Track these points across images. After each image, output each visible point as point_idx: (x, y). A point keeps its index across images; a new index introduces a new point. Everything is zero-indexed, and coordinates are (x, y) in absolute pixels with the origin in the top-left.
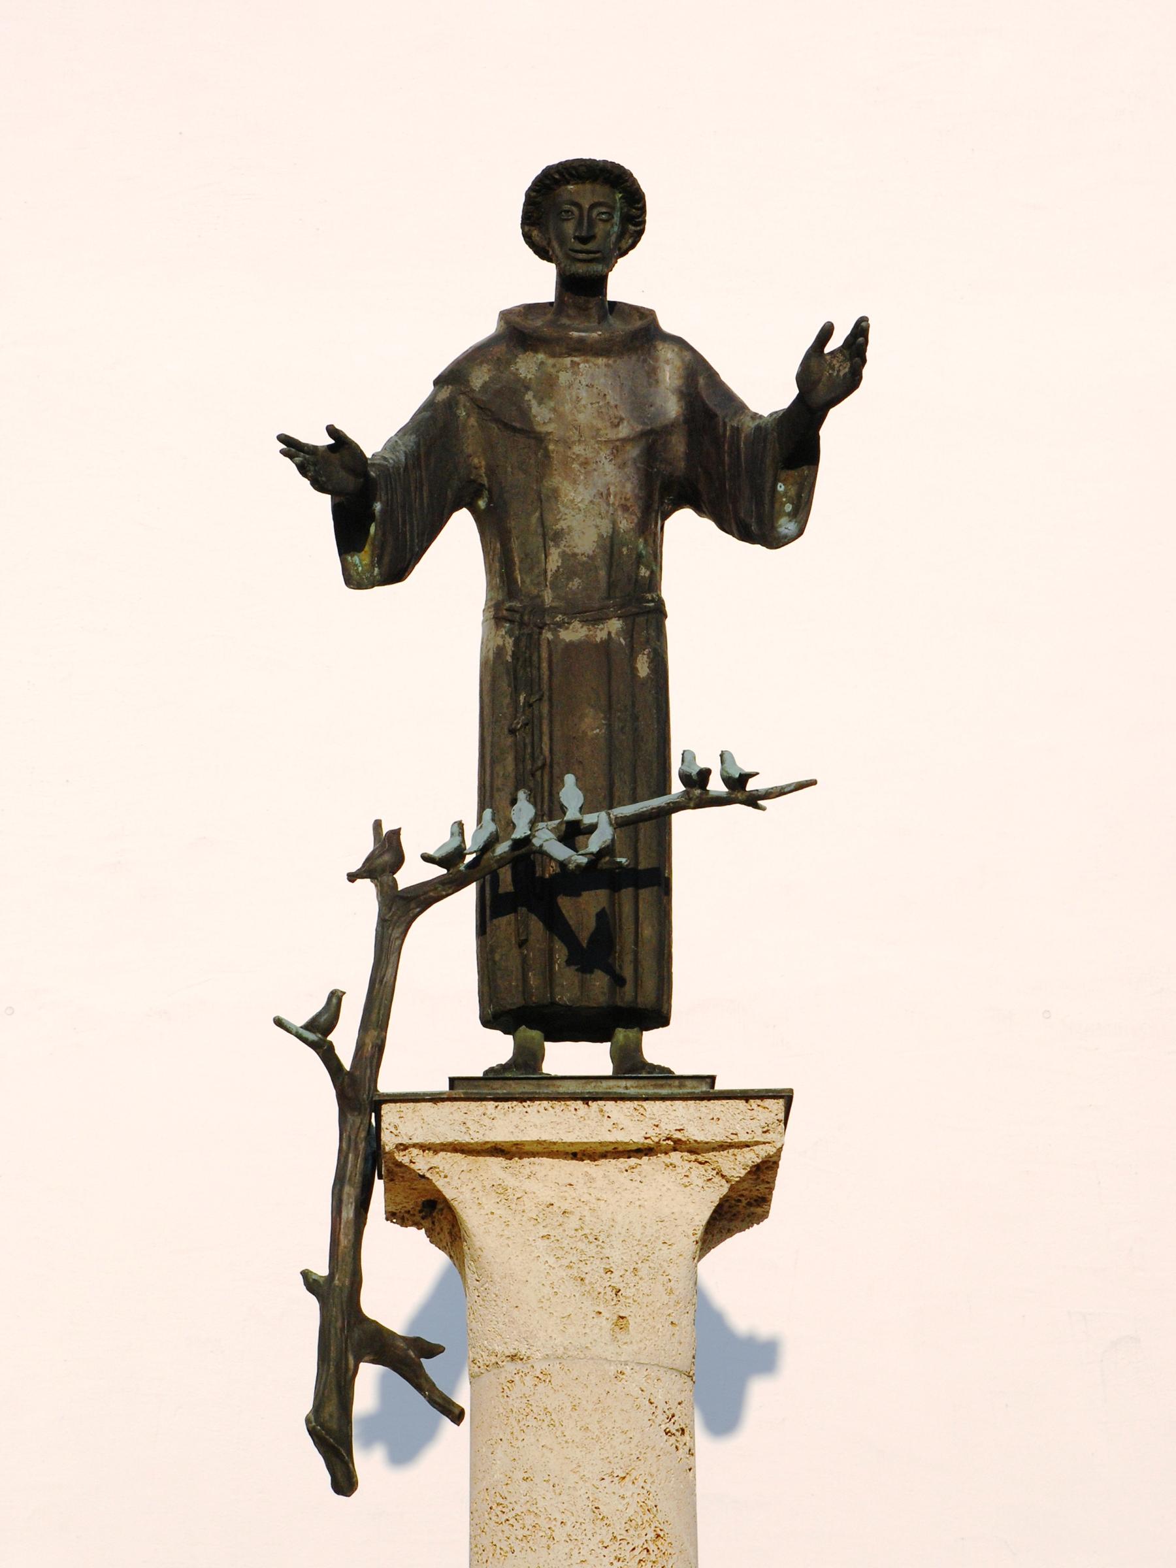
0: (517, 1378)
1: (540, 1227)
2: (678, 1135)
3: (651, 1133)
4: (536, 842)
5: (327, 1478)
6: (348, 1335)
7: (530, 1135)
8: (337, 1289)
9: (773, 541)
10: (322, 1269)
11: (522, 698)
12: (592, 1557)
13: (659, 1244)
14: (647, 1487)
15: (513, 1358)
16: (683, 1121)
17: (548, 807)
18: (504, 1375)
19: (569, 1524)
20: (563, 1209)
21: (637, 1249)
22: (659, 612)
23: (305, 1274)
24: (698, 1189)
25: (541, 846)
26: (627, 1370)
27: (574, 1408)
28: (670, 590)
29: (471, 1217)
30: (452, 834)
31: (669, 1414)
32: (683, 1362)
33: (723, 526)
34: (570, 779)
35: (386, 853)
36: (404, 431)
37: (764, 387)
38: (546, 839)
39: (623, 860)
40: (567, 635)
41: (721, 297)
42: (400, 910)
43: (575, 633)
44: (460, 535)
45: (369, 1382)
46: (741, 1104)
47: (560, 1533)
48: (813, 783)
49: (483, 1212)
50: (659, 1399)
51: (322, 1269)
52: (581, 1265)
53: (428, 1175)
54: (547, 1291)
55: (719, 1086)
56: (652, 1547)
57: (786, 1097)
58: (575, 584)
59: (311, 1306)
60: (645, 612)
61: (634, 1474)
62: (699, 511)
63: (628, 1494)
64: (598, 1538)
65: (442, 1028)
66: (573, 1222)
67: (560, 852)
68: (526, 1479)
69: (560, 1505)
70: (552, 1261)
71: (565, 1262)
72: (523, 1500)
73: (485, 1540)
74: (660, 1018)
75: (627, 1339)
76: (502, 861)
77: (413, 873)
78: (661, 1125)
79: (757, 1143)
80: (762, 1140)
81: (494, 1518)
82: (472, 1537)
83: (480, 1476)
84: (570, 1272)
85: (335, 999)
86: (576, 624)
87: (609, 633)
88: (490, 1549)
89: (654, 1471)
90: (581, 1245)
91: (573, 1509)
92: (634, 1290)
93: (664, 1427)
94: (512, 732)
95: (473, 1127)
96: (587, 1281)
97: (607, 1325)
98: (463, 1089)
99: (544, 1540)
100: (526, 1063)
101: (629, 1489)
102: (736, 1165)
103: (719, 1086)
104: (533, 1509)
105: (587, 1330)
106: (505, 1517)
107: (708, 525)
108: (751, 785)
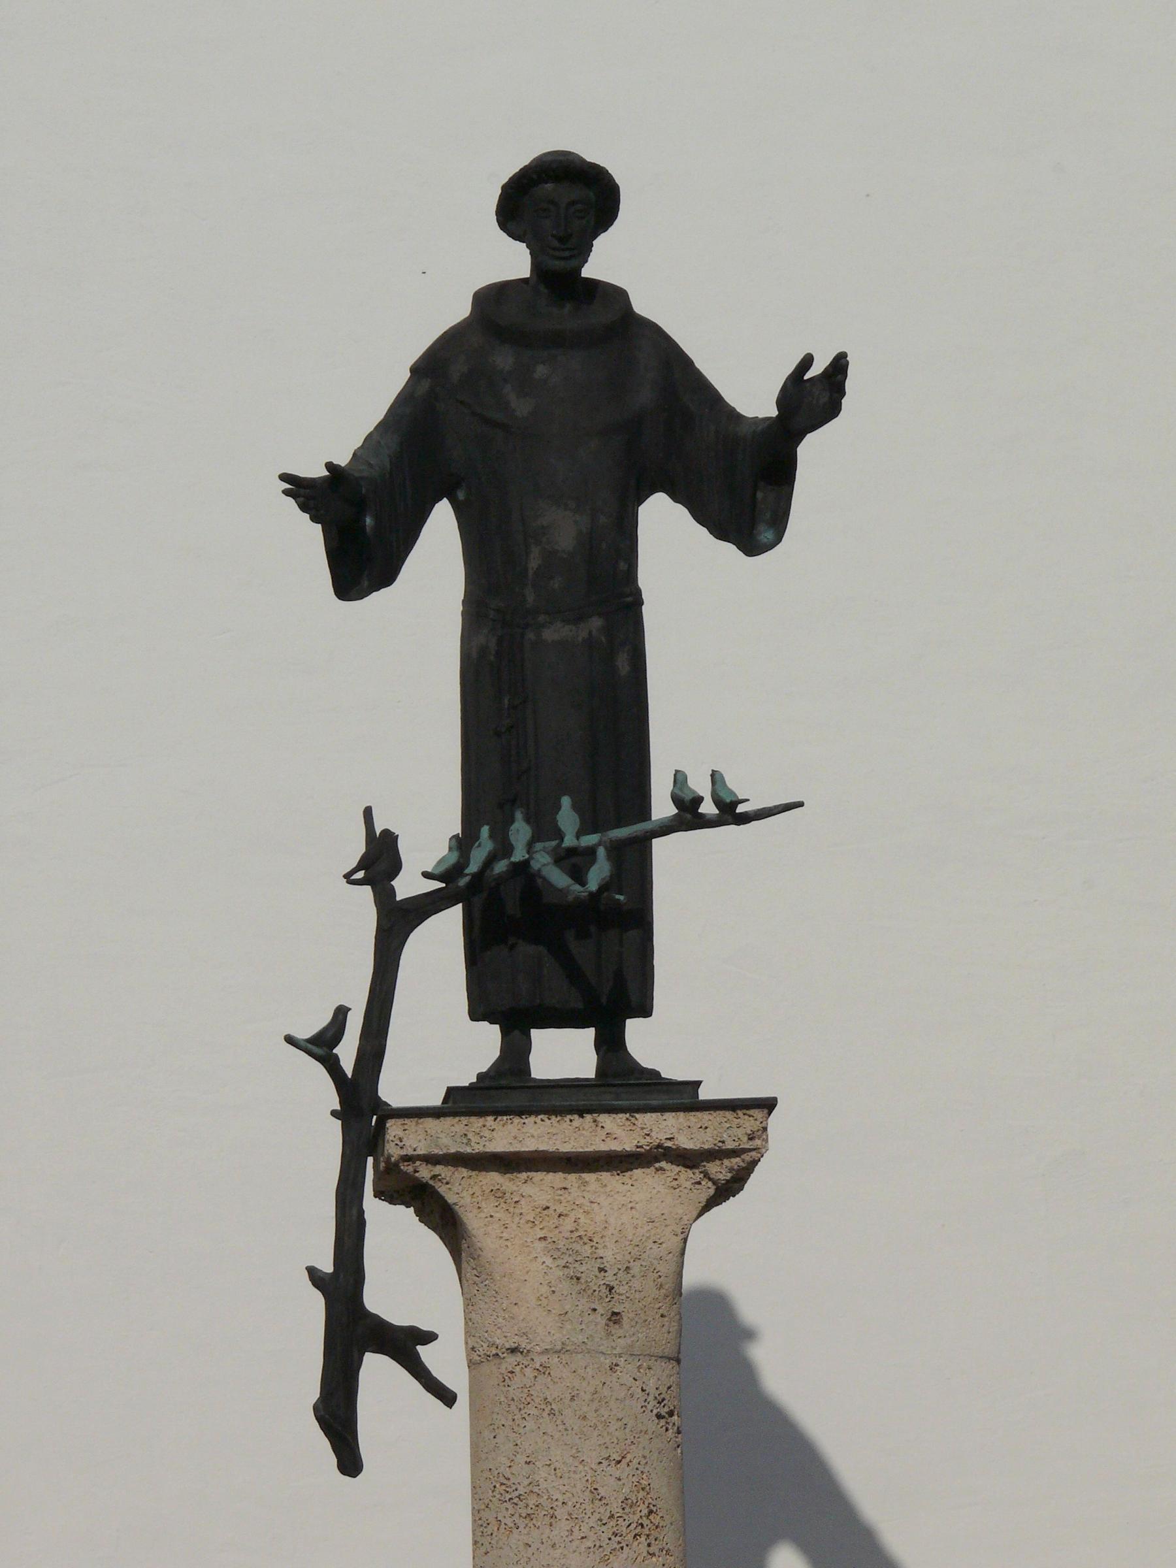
0: (518, 1369)
1: (537, 1228)
2: (669, 1144)
3: (643, 1142)
4: (535, 865)
5: (333, 1460)
6: (355, 1333)
7: (529, 1145)
8: (342, 1285)
9: (751, 547)
10: (327, 1265)
11: (506, 701)
12: (592, 1534)
13: (650, 1244)
14: (641, 1468)
15: (513, 1351)
16: (674, 1130)
17: (545, 829)
18: (503, 1366)
19: (570, 1504)
20: (559, 1211)
21: (629, 1249)
22: (635, 602)
23: (313, 1273)
24: (686, 1191)
25: (539, 870)
26: (621, 1361)
27: (572, 1399)
28: (646, 578)
29: (472, 1221)
30: (450, 849)
31: (660, 1399)
32: (669, 1350)
33: (701, 517)
34: (566, 801)
35: (379, 859)
36: (383, 426)
37: (753, 396)
38: (542, 861)
39: (621, 898)
40: (549, 635)
41: (707, 289)
42: (397, 922)
43: (555, 632)
44: (441, 534)
45: (378, 1373)
46: (729, 1115)
47: (561, 1513)
48: (800, 805)
49: (483, 1215)
50: (651, 1386)
51: (327, 1265)
52: (577, 1265)
53: (431, 1182)
54: (544, 1290)
55: (704, 1094)
56: (645, 1522)
57: (768, 1105)
58: (556, 583)
59: (316, 1303)
60: (621, 606)
61: (629, 1457)
62: (676, 499)
63: (624, 1476)
64: (598, 1516)
65: (439, 1042)
66: (568, 1224)
67: (559, 878)
68: (528, 1463)
69: (561, 1487)
70: (549, 1261)
71: (562, 1263)
72: (526, 1482)
73: (489, 1515)
74: (645, 1011)
75: (621, 1332)
76: (501, 879)
77: (409, 884)
78: (653, 1134)
79: (745, 1151)
80: (747, 1146)
81: (501, 1504)
82: (476, 1512)
83: (483, 1456)
84: (566, 1271)
85: (341, 1014)
86: (559, 624)
87: (590, 632)
88: (494, 1522)
89: (646, 1453)
90: (576, 1247)
91: (574, 1491)
92: (626, 1287)
93: (655, 1412)
94: (498, 734)
95: (474, 1139)
96: (582, 1281)
97: (603, 1321)
98: (461, 1102)
99: (547, 1519)
100: (515, 1054)
101: (623, 1471)
102: (720, 1170)
103: (704, 1094)
104: (536, 1489)
105: (583, 1326)
106: (508, 1496)
107: (681, 513)
108: (740, 809)
